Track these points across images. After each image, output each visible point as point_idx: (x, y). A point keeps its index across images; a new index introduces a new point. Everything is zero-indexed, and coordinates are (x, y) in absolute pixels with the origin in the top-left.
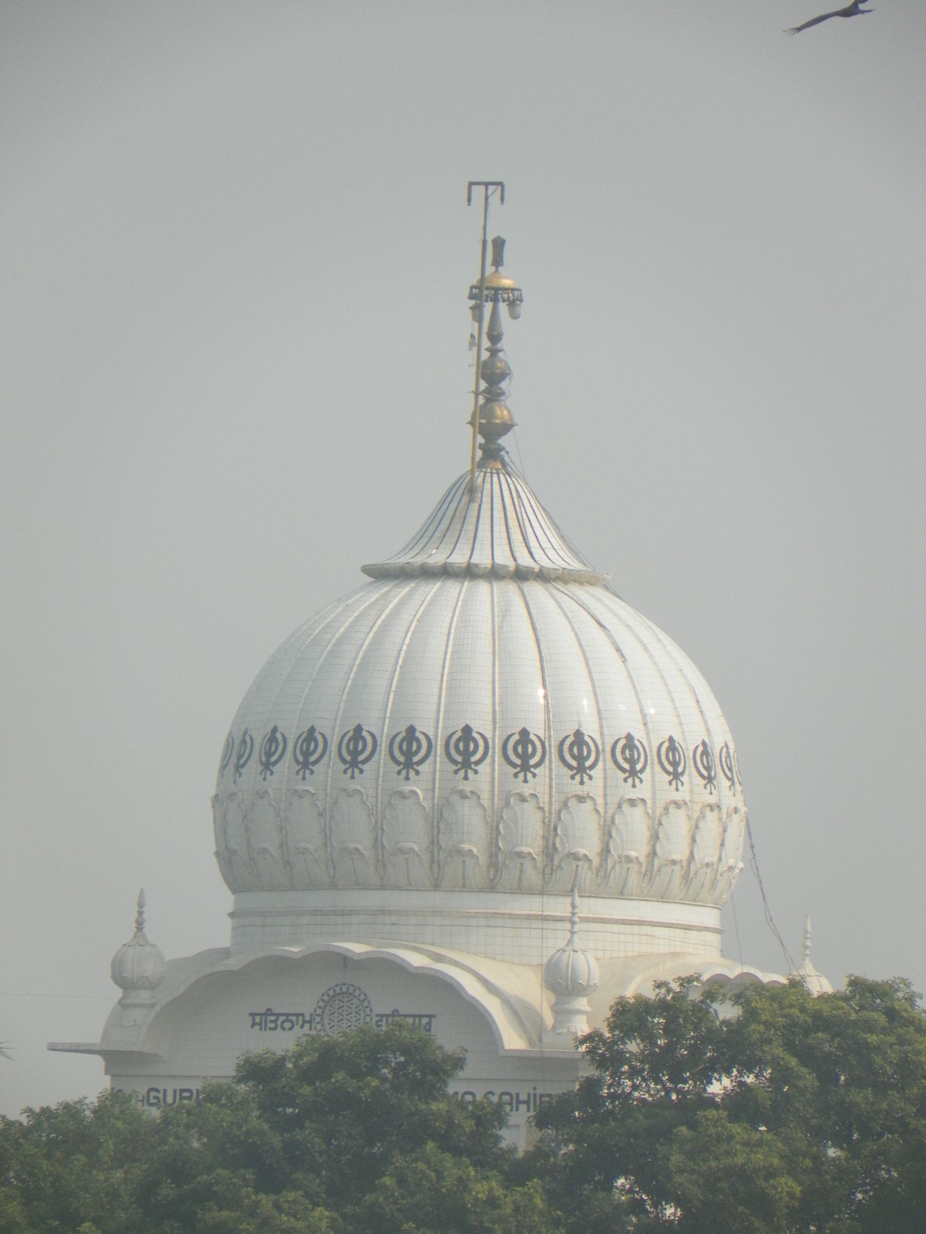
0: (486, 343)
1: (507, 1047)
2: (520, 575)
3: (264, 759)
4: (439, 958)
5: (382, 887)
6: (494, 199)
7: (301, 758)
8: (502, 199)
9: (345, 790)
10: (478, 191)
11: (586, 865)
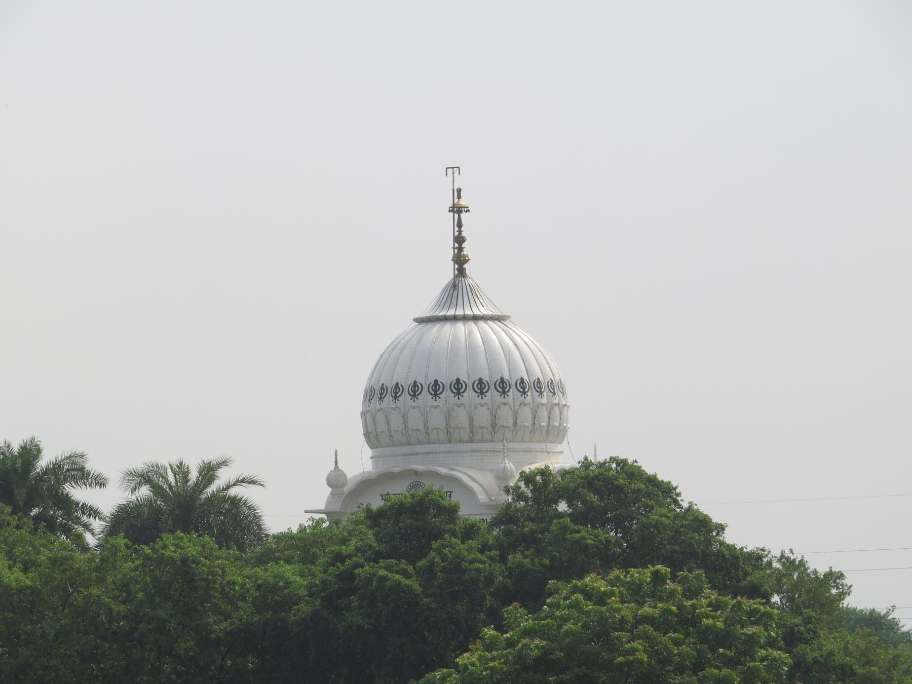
0: (456, 229)
4: (452, 469)
5: (429, 443)
6: (456, 173)
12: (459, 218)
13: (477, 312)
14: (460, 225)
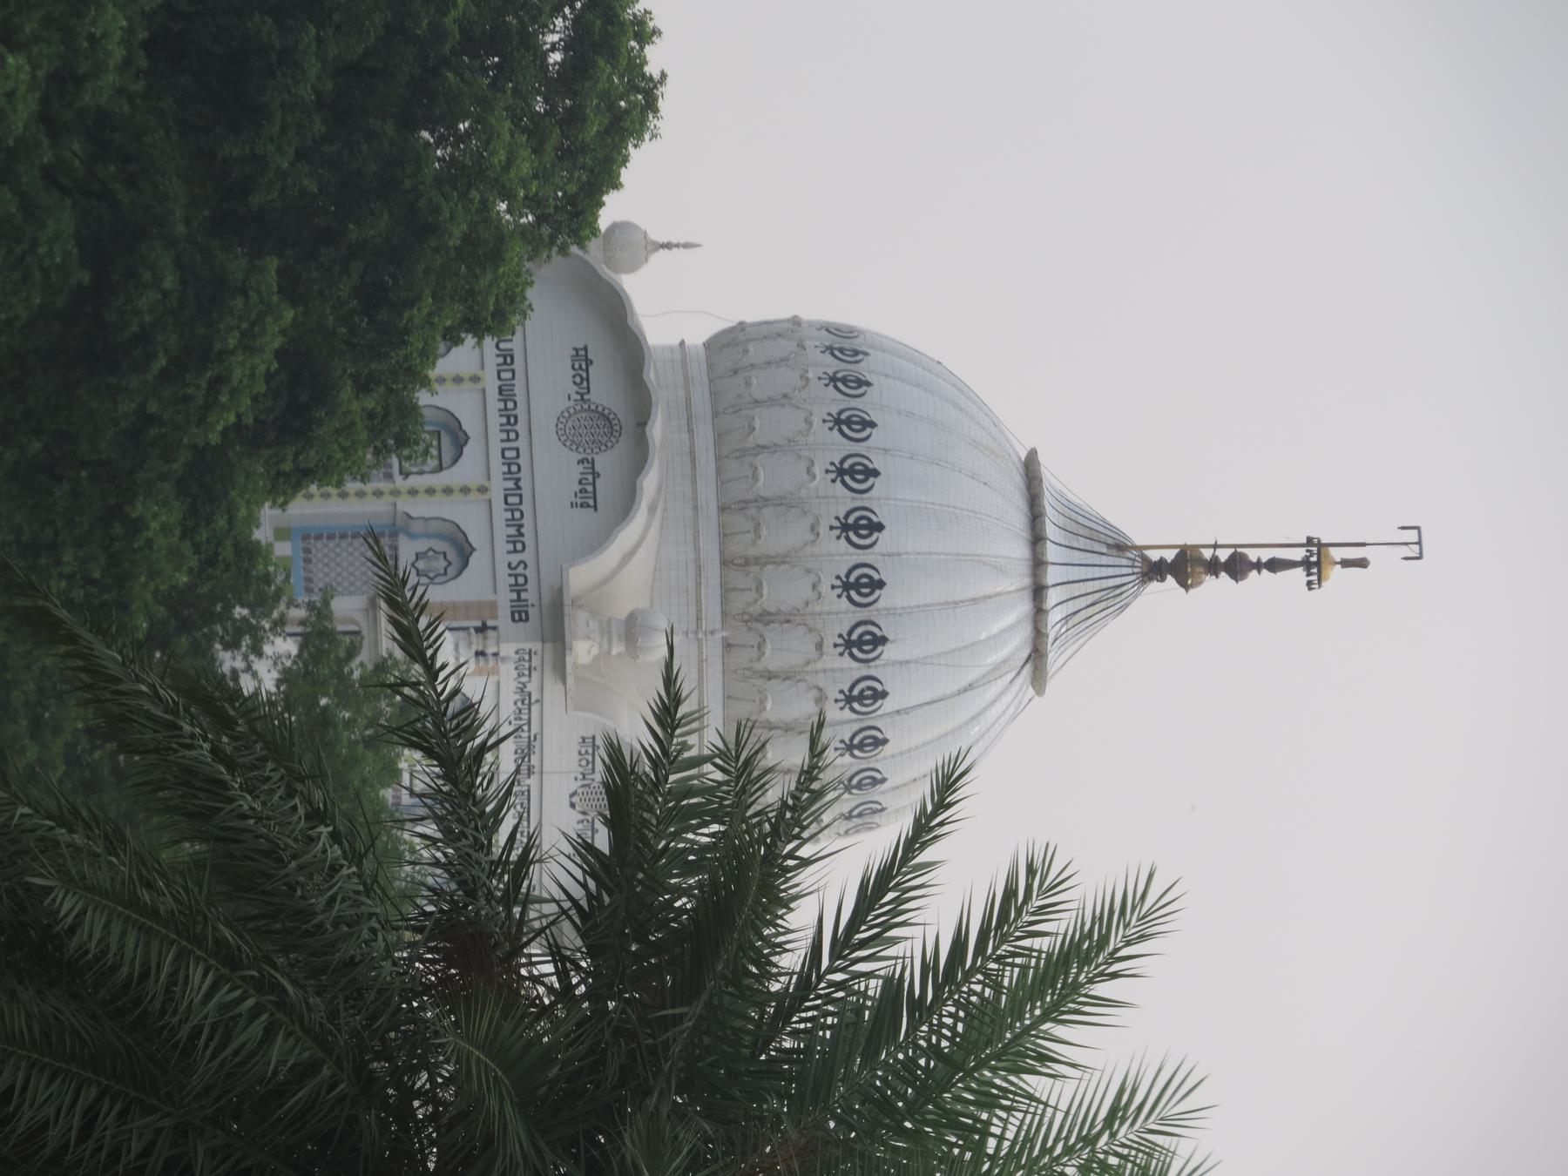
1: (572, 571)
2: (1038, 591)
3: (839, 375)
4: (652, 510)
5: (718, 458)
7: (843, 417)
8: (1407, 558)
9: (813, 463)
11: (755, 656)
12: (1291, 564)
13: (1053, 597)
14: (1274, 565)
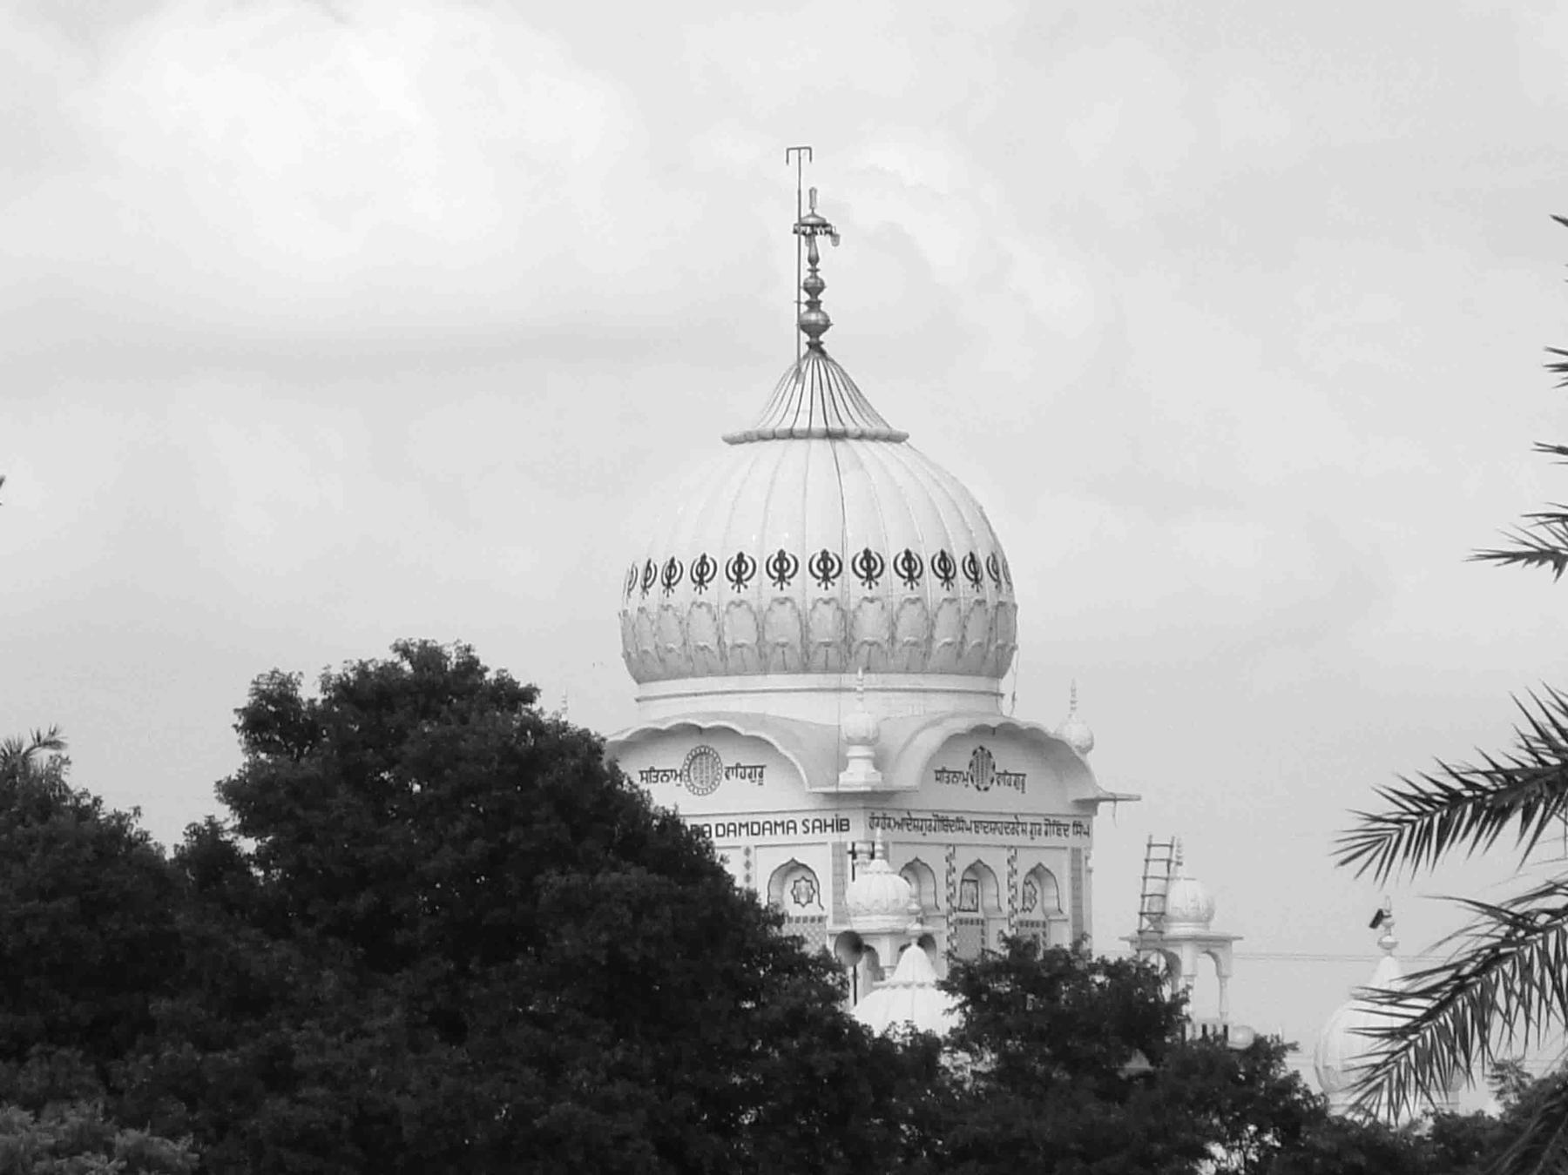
0: (806, 265)
10: (794, 155)
